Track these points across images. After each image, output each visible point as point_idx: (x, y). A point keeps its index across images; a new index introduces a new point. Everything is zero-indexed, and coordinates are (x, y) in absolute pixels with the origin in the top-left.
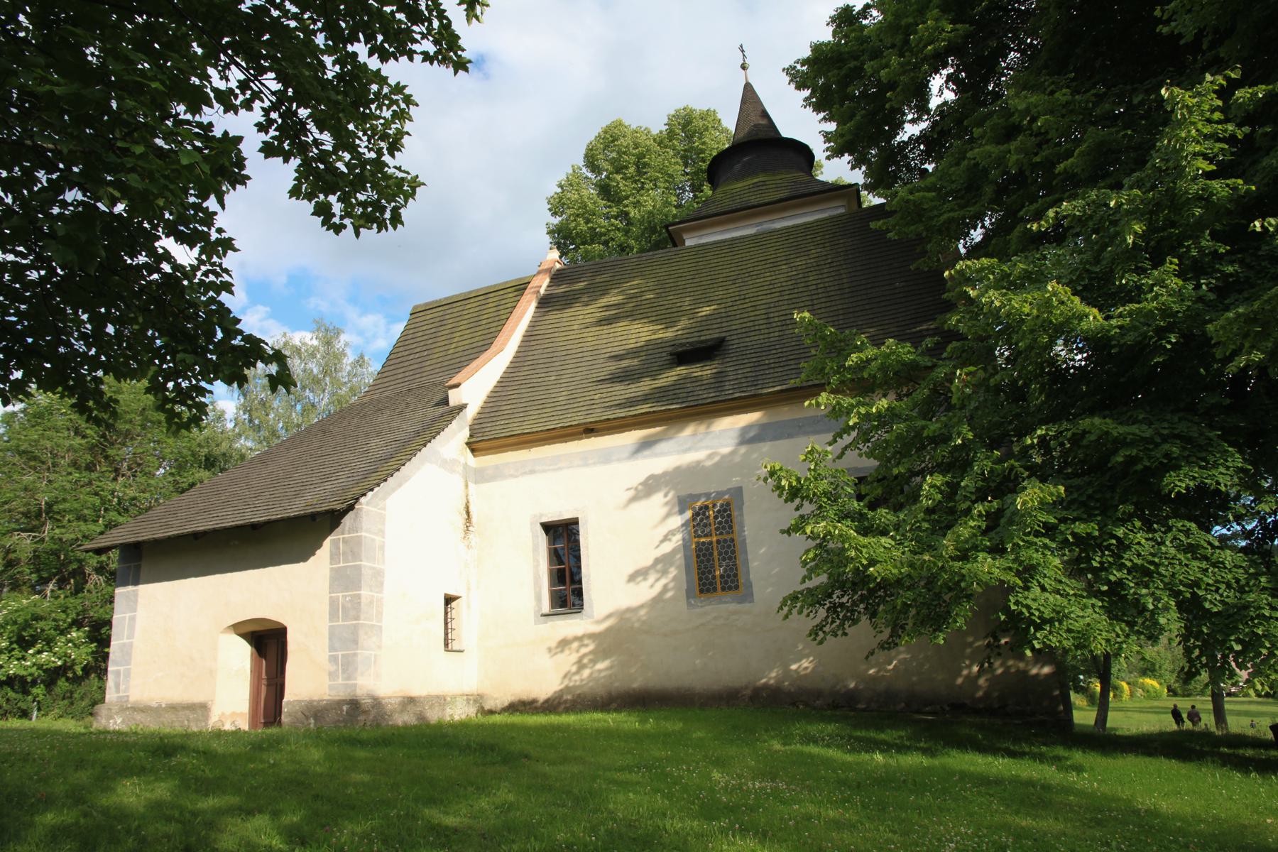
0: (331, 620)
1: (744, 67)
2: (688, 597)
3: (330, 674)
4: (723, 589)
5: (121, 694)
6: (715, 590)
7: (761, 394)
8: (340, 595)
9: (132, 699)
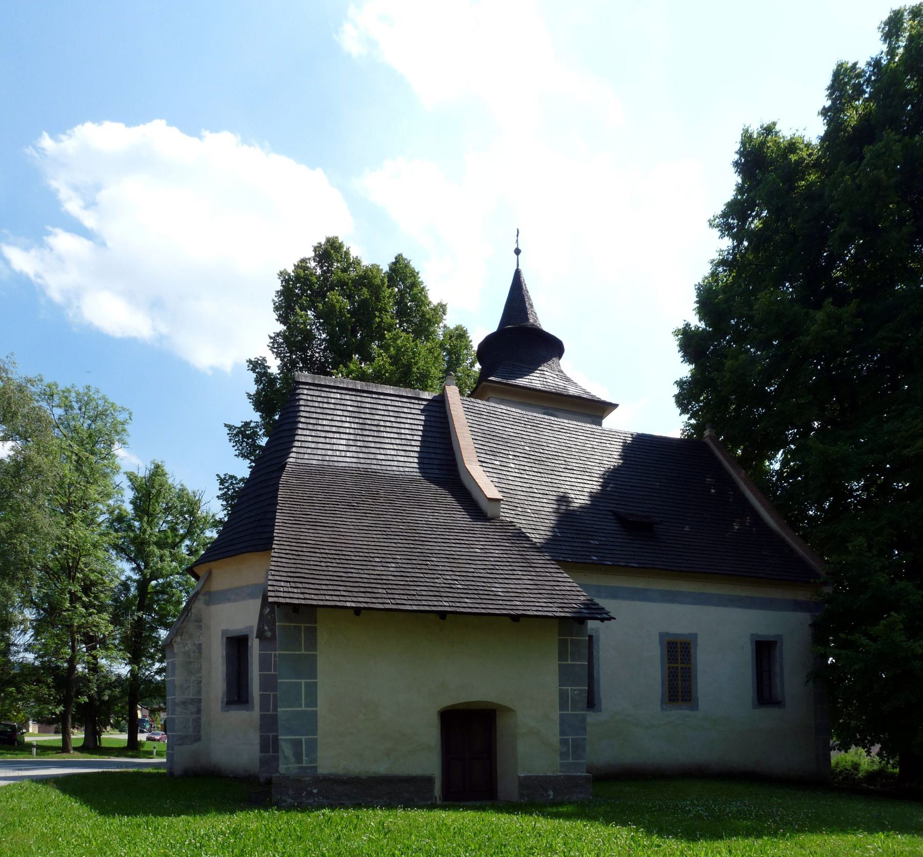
0: (561, 709)
1: (518, 252)
2: (662, 704)
4: (682, 700)
5: (304, 765)
6: (678, 700)
7: (605, 564)
8: (569, 688)
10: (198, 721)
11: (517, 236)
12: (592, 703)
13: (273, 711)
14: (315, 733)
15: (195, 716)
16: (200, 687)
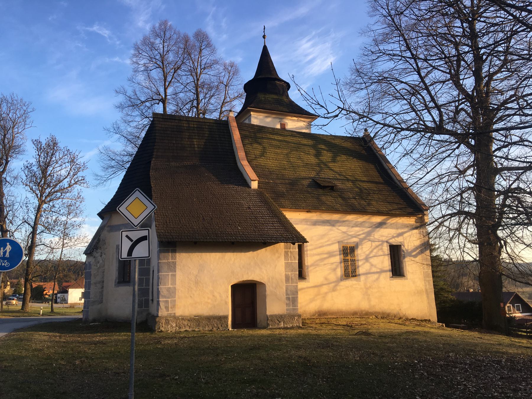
0: (286, 283)
1: (264, 37)
3: (287, 304)
5: (169, 312)
8: (290, 273)
10: (102, 292)
11: (264, 29)
12: (302, 276)
13: (171, 285)
16: (104, 275)
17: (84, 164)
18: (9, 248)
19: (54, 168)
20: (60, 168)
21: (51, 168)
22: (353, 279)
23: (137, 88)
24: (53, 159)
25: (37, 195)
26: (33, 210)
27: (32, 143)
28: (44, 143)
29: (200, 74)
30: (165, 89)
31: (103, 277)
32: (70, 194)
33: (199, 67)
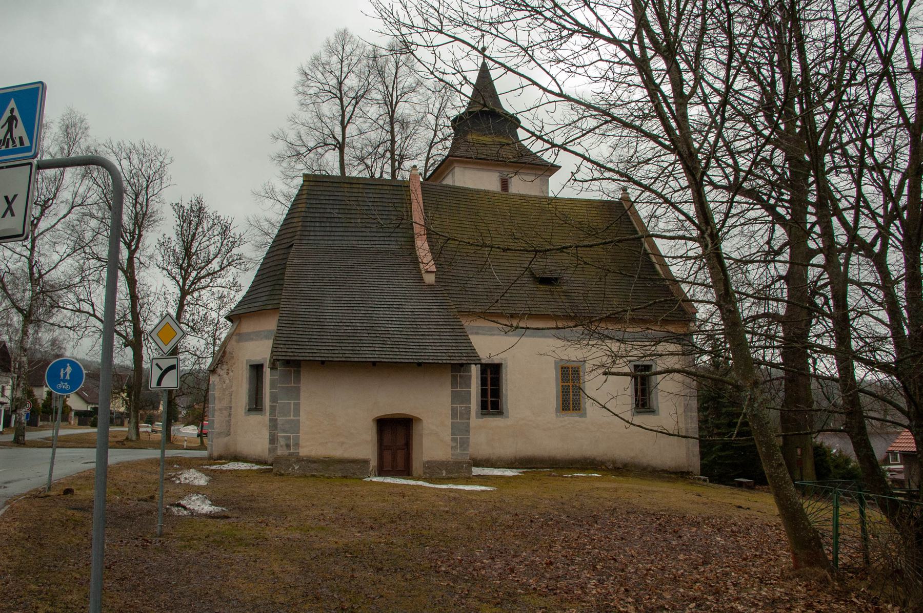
0: (452, 419)
9: (301, 454)
14: (298, 432)
15: (227, 419)
17: (240, 236)
18: (69, 369)
19: (200, 244)
20: (208, 243)
21: (197, 244)
22: (575, 413)
23: (303, 131)
24: (198, 231)
25: (178, 282)
26: (173, 304)
27: (171, 207)
28: (187, 207)
29: (348, 122)
30: (344, 128)
31: (230, 402)
32: (223, 280)
33: (395, 93)
